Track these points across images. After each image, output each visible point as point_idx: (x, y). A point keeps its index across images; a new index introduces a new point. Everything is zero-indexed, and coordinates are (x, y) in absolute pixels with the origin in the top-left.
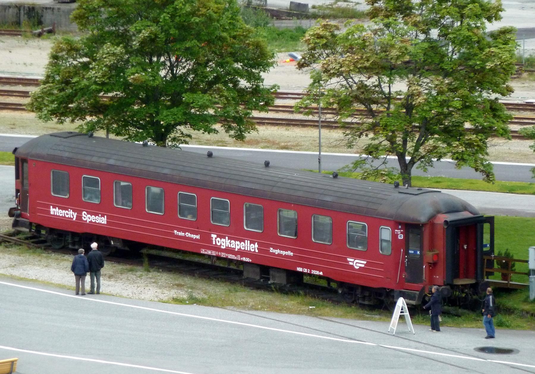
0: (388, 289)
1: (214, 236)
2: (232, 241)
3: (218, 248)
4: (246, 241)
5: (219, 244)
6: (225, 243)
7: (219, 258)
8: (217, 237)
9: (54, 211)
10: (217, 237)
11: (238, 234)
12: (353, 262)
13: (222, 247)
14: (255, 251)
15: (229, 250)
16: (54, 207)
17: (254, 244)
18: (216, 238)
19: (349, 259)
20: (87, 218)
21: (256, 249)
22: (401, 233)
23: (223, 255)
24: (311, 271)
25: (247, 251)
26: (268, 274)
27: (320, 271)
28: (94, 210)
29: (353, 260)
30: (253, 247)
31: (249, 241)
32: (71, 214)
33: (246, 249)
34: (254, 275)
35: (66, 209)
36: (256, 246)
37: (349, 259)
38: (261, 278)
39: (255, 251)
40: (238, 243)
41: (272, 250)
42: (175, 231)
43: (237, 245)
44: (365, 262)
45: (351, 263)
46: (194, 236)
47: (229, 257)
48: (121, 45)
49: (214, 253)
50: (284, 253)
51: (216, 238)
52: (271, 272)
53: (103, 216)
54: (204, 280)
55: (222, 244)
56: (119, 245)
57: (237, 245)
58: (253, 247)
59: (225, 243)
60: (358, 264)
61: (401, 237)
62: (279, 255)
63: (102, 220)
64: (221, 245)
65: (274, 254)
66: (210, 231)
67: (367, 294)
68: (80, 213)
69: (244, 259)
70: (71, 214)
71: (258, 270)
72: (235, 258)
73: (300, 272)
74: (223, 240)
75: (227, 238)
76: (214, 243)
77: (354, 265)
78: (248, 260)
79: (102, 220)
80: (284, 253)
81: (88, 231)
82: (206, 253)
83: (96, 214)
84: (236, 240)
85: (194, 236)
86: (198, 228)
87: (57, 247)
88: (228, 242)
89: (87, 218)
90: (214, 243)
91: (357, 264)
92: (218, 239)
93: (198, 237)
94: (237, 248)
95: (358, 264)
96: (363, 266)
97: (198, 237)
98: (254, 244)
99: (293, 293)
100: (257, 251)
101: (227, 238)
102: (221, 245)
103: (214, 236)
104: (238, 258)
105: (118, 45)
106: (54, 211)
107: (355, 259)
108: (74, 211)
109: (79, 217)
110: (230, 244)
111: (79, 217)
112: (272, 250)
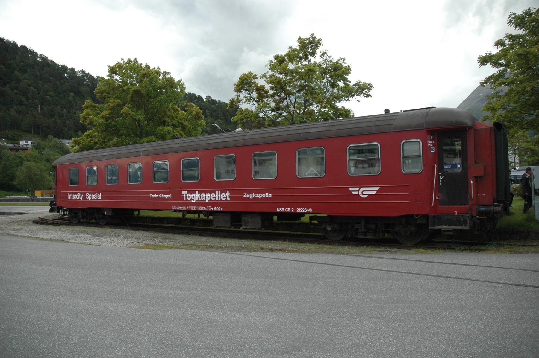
0: (417, 216)
1: (184, 193)
2: (203, 194)
3: (189, 203)
4: (217, 192)
5: (189, 199)
6: (194, 197)
7: (189, 212)
8: (188, 193)
9: (71, 196)
10: (188, 193)
11: (208, 186)
12: (358, 191)
13: (192, 201)
14: (226, 200)
15: (199, 203)
16: (70, 194)
17: (226, 193)
18: (186, 194)
19: (351, 189)
20: (89, 197)
21: (228, 197)
22: (434, 145)
23: (194, 208)
24: (295, 210)
25: (218, 200)
26: (240, 221)
27: (308, 208)
28: (93, 190)
29: (357, 189)
30: (225, 196)
31: (220, 191)
32: (80, 196)
33: (217, 199)
34: (224, 224)
35: (76, 193)
36: (228, 194)
37: (351, 189)
38: (232, 225)
39: (226, 200)
40: (209, 194)
41: (245, 195)
42: (151, 195)
43: (207, 197)
44: (377, 188)
45: (354, 193)
46: (167, 196)
47: (199, 209)
48: (270, 85)
49: (185, 208)
50: (260, 196)
51: (186, 194)
52: (243, 218)
53: (99, 193)
54: (437, 251)
55: (193, 198)
56: (110, 214)
57: (207, 197)
58: (225, 196)
59: (194, 197)
60: (365, 192)
61: (433, 150)
62: (254, 199)
63: (98, 197)
64: (191, 199)
65: (248, 199)
66: (181, 188)
67: (85, 214)
68: (84, 194)
69: (215, 209)
70: (80, 196)
71: (228, 218)
72: (206, 209)
73: (282, 213)
74: (193, 195)
75: (197, 192)
76: (185, 199)
77: (360, 194)
78: (219, 209)
79: (98, 197)
80: (260, 196)
81: (90, 206)
82: (177, 209)
83: (94, 193)
84: (205, 192)
85: (167, 196)
86: (169, 189)
87: (104, 223)
88: (198, 195)
89: (89, 197)
90: (185, 199)
91: (364, 193)
92: (189, 195)
93: (170, 196)
94: (207, 200)
95: (365, 192)
96: (374, 193)
97: (170, 196)
98: (226, 193)
99: (126, 225)
100: (228, 199)
101: (197, 192)
102: (191, 199)
103: (184, 193)
104: (209, 208)
105: (269, 83)
106: (71, 196)
107: (361, 187)
108: (81, 194)
109: (84, 198)
110: (200, 196)
111: (84, 198)
112: (245, 195)
